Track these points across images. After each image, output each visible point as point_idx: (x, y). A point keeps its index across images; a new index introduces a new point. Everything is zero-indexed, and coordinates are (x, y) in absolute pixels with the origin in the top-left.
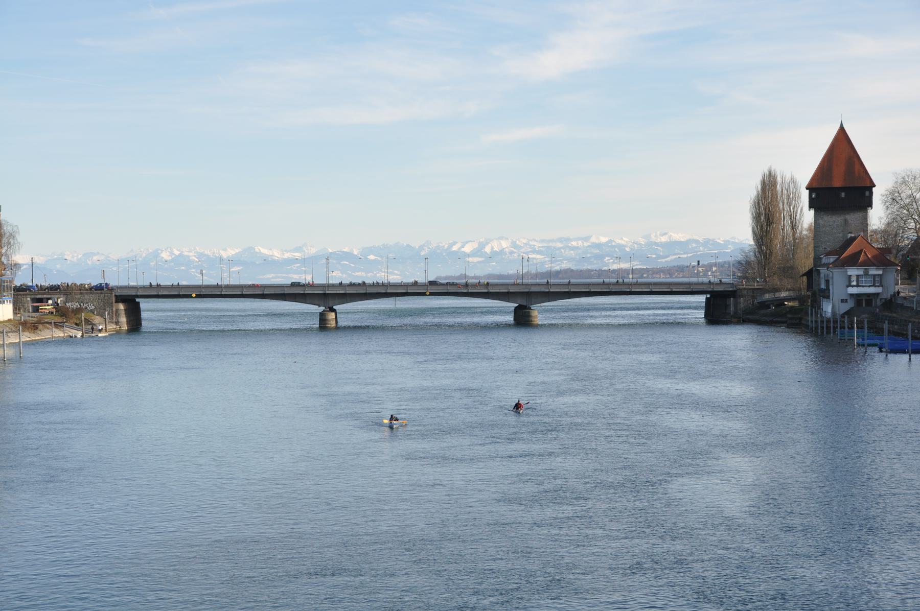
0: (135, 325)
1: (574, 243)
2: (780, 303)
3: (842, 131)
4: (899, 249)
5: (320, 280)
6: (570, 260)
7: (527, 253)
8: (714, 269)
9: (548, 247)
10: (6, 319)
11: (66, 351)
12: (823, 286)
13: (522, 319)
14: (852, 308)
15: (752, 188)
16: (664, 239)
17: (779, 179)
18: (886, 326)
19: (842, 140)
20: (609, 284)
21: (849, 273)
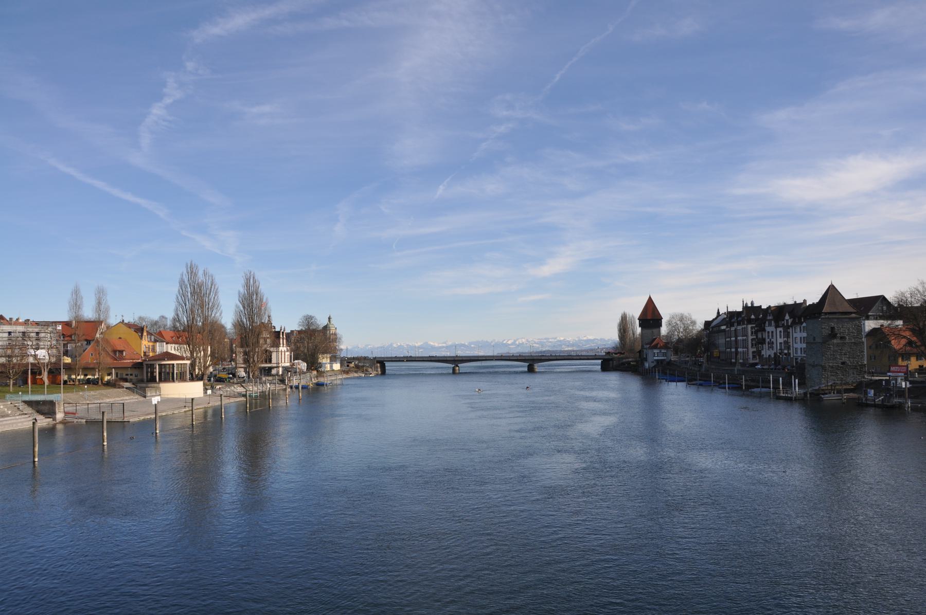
0: (383, 372)
1: (551, 340)
2: (629, 363)
3: (650, 298)
4: (672, 343)
5: (453, 355)
6: (549, 346)
7: (533, 344)
9: (540, 342)
10: (338, 369)
11: (358, 382)
12: (645, 357)
13: (531, 370)
15: (618, 320)
16: (585, 338)
17: (628, 316)
18: (668, 372)
19: (650, 302)
20: (548, 356)
21: (654, 351)
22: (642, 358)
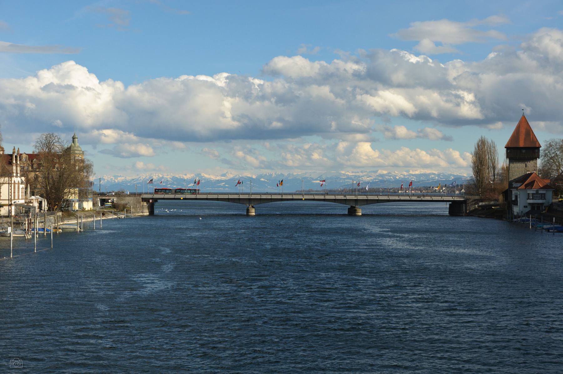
8: (444, 189)
9: (355, 176)
14: (530, 211)
21: (528, 192)
22: (510, 202)
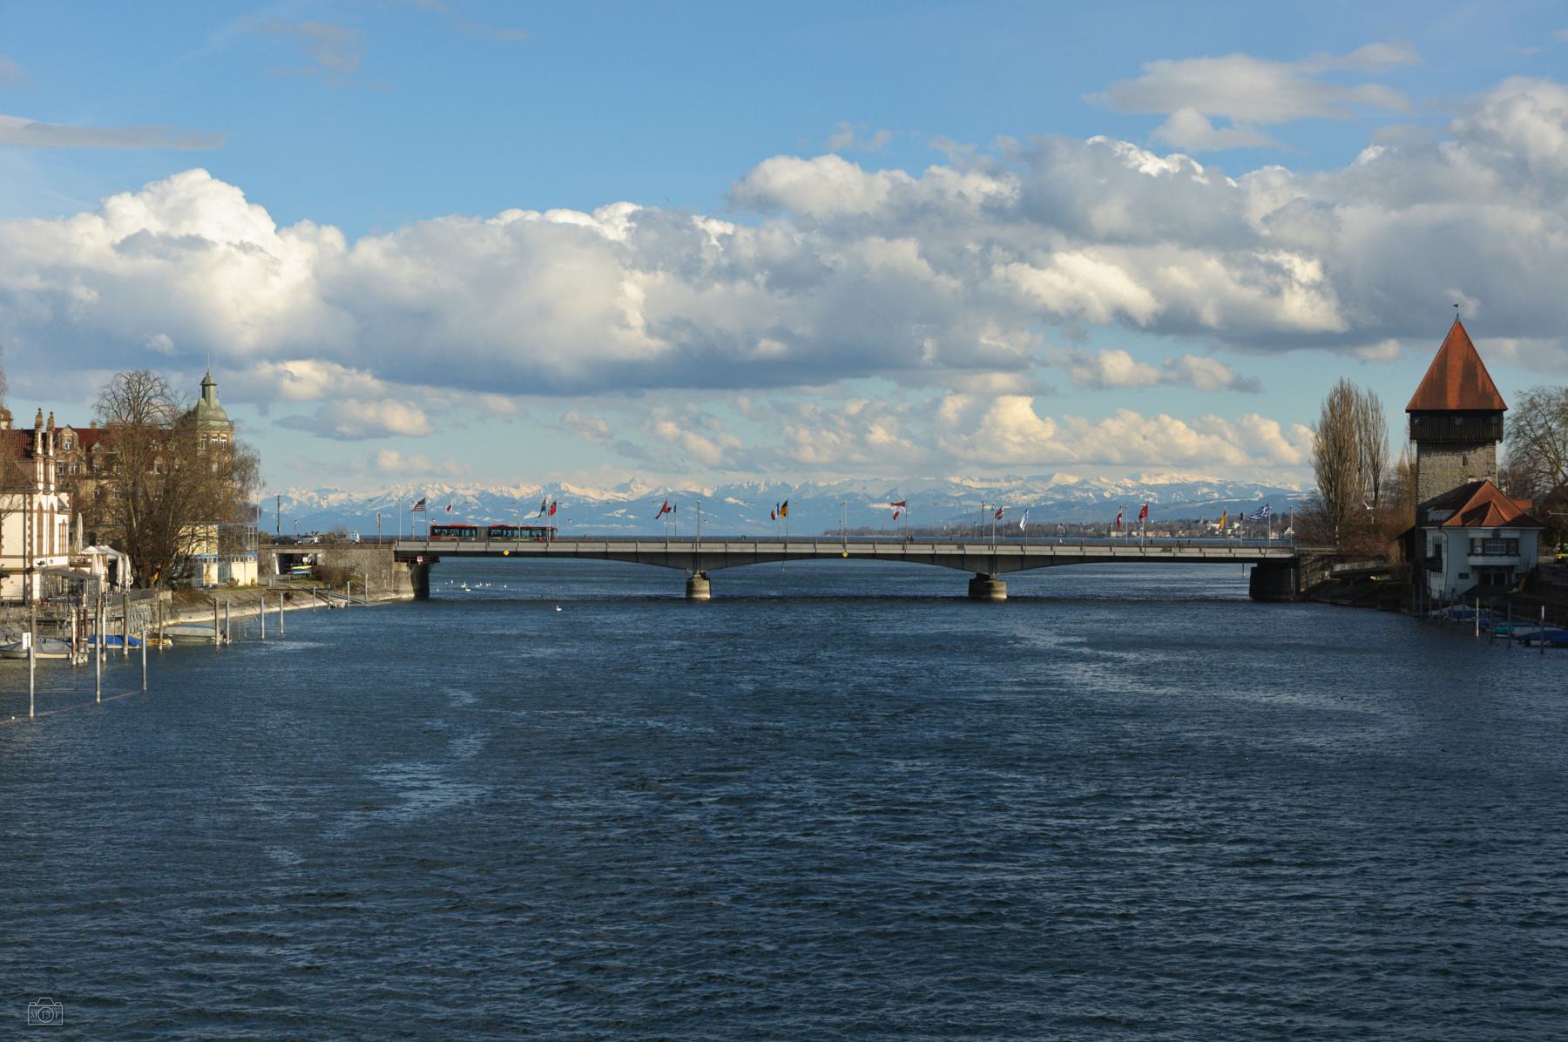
8: (1236, 525)
9: (990, 490)
14: (1475, 587)
21: (1472, 535)
22: (1420, 564)
